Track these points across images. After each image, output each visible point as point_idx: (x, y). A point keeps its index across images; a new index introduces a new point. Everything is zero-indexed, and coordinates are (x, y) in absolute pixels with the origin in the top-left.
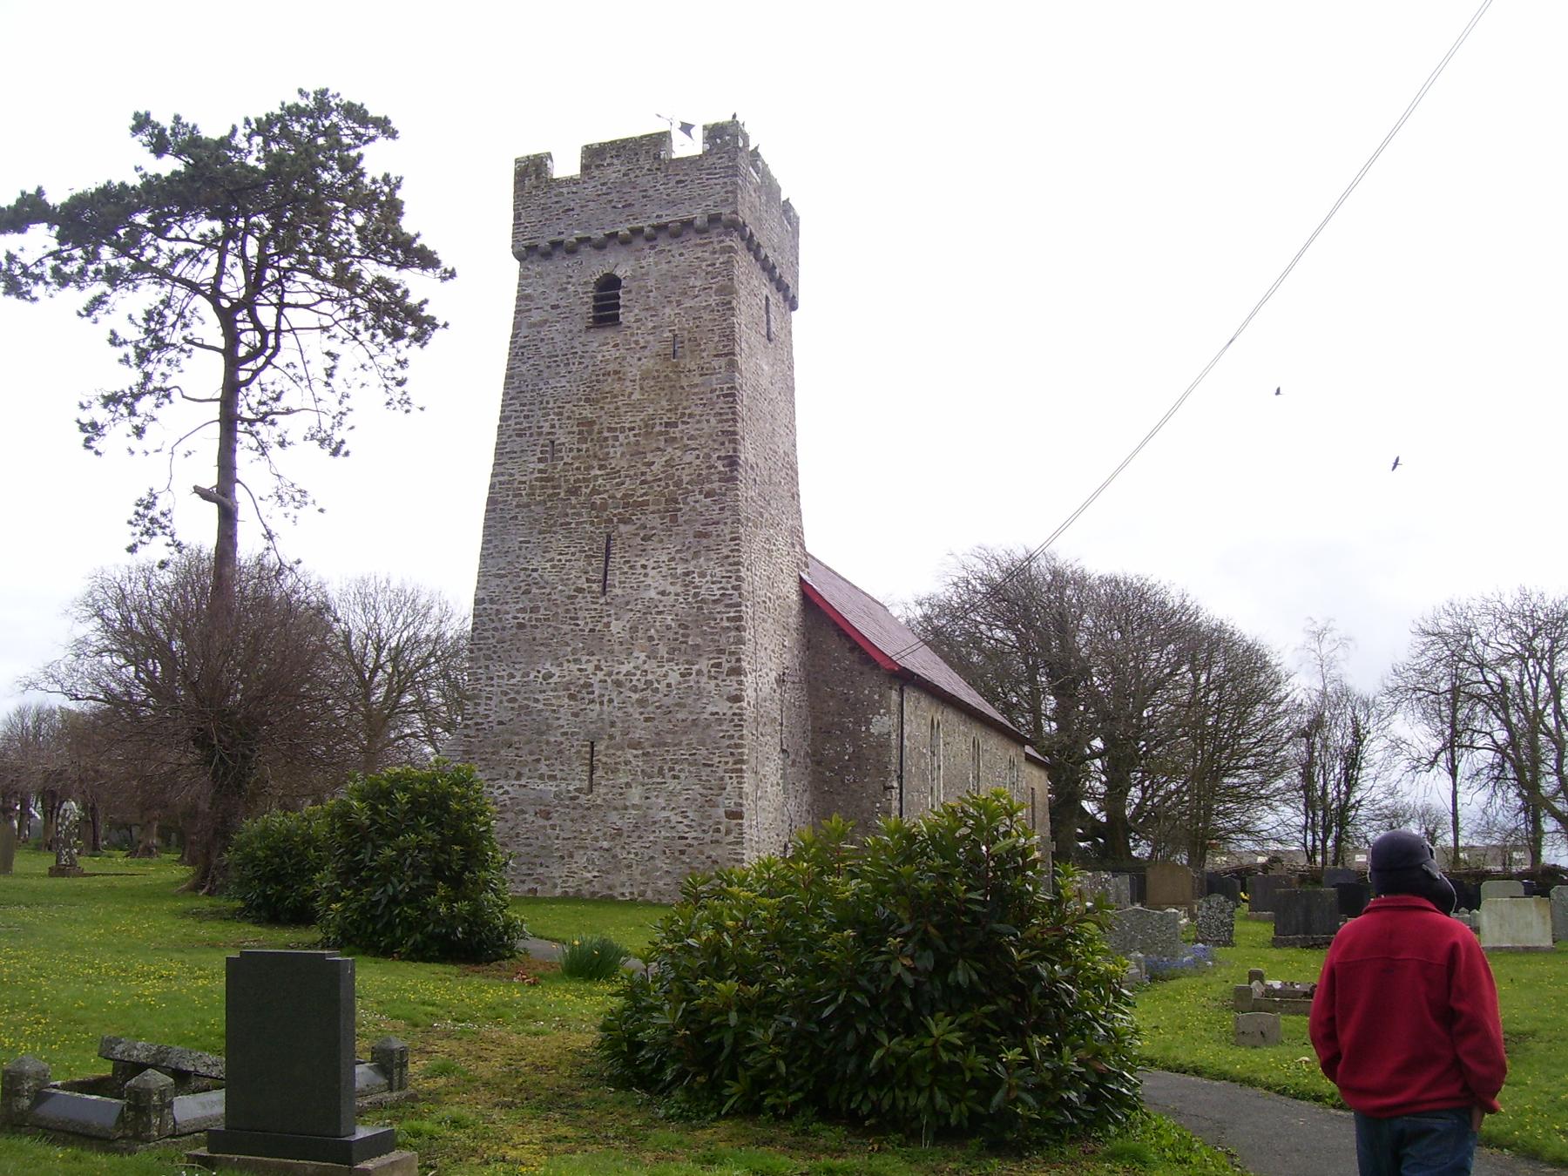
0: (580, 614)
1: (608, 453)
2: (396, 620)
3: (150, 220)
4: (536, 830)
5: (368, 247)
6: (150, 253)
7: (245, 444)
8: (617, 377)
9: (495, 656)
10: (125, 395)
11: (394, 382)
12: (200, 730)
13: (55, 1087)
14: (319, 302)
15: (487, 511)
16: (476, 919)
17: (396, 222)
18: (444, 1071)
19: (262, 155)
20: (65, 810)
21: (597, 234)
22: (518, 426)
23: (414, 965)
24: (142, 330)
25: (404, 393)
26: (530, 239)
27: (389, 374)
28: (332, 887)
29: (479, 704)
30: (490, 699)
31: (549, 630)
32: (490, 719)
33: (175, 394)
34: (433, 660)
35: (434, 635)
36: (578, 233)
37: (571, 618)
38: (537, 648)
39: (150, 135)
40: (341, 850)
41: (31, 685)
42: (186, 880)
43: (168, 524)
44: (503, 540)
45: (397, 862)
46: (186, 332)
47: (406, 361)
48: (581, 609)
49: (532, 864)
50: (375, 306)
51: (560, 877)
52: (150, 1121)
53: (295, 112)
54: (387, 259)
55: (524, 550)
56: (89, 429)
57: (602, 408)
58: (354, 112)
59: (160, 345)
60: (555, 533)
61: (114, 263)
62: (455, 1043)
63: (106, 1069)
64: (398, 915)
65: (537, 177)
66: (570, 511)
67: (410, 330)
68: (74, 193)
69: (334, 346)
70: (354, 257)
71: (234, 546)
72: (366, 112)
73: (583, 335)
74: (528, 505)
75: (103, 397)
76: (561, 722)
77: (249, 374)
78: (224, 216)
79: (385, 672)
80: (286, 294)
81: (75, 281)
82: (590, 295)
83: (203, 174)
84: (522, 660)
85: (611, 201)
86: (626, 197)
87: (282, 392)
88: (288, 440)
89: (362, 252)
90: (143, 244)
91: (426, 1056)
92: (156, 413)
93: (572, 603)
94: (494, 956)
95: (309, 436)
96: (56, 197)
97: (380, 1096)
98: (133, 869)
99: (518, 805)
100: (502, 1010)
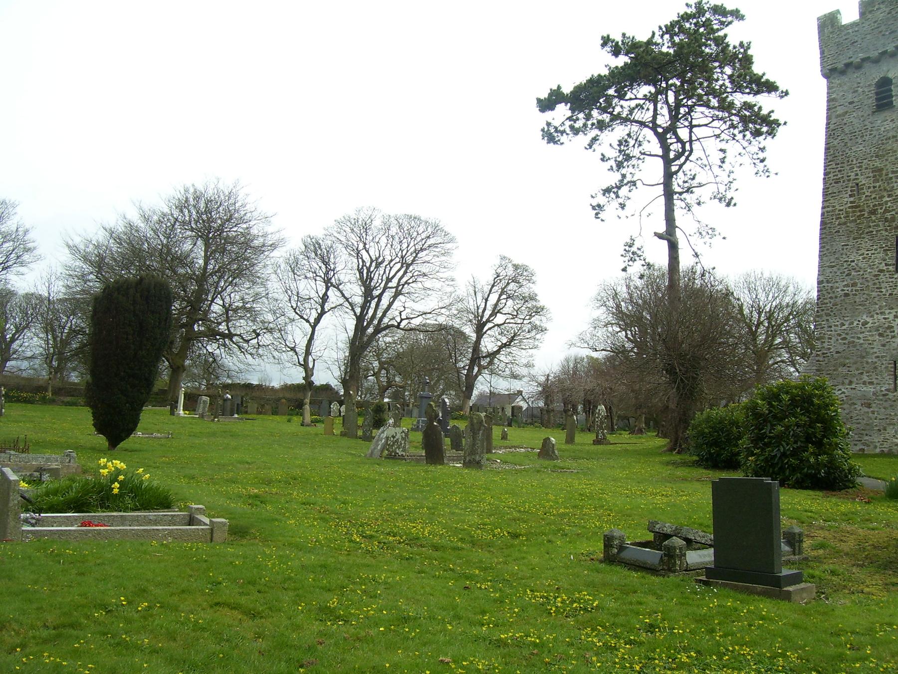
0: (883, 285)
1: (893, 187)
2: (768, 295)
3: (616, 91)
4: (863, 415)
5: (736, 86)
6: (617, 110)
7: (678, 206)
8: (894, 139)
9: (832, 314)
10: (613, 188)
11: (759, 161)
12: (669, 364)
13: (628, 544)
14: (712, 122)
15: (821, 229)
16: (832, 465)
17: (749, 68)
18: (822, 546)
19: (670, 44)
20: (599, 410)
21: (874, 54)
22: (835, 177)
23: (797, 491)
24: (617, 151)
25: (765, 166)
26: (831, 65)
27: (755, 156)
28: (748, 448)
29: (824, 342)
30: (831, 339)
31: (864, 296)
32: (831, 351)
33: (639, 184)
34: (791, 317)
35: (791, 302)
36: (861, 55)
37: (877, 288)
38: (857, 307)
39: (611, 47)
40: (753, 428)
41: (572, 345)
42: (665, 446)
43: (642, 254)
44: (832, 245)
45: (785, 434)
46: (641, 148)
47: (764, 148)
48: (883, 282)
49: (861, 434)
50: (745, 120)
51: (879, 442)
52: (675, 562)
53: (686, 17)
54: (748, 91)
55: (845, 250)
56: (597, 208)
57: (887, 160)
58: (719, 10)
59: (628, 158)
60: (864, 238)
61: (600, 118)
62: (826, 532)
63: (650, 537)
64: (787, 462)
65: (832, 26)
66: (871, 224)
67: (765, 129)
68: (576, 85)
69: (723, 145)
70: (728, 93)
71: (678, 263)
72: (725, 8)
73: (870, 117)
74: (845, 223)
75: (603, 190)
76: (875, 350)
77: (677, 167)
78: (653, 82)
79: (764, 326)
80: (693, 120)
81: (582, 131)
82: (873, 92)
83: (641, 62)
84: (848, 315)
85: (881, 32)
86: (891, 27)
87: (695, 175)
88: (702, 201)
89: (733, 89)
90: (614, 105)
91: (811, 539)
92: (630, 195)
93: (877, 279)
94: (843, 487)
95: (713, 197)
96: (567, 89)
97: (789, 557)
98: (635, 441)
99: (851, 400)
100: (851, 516)
